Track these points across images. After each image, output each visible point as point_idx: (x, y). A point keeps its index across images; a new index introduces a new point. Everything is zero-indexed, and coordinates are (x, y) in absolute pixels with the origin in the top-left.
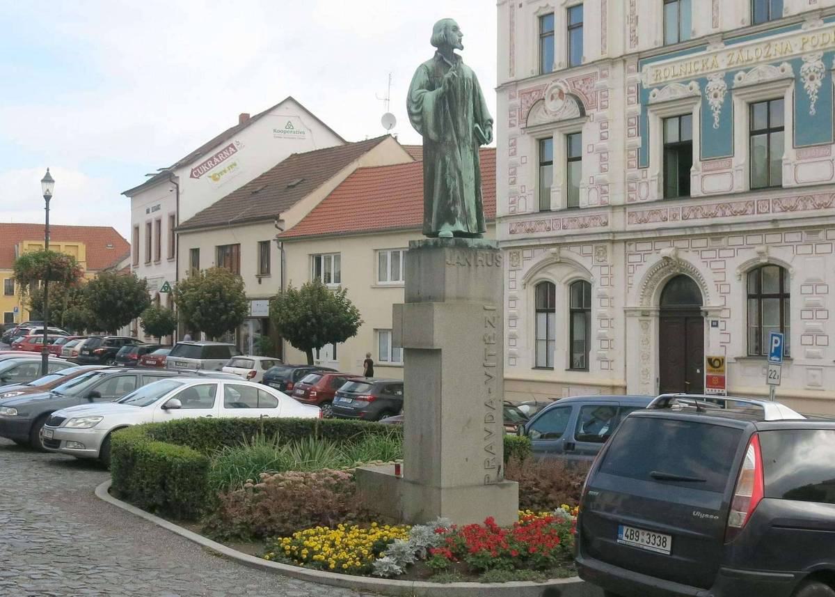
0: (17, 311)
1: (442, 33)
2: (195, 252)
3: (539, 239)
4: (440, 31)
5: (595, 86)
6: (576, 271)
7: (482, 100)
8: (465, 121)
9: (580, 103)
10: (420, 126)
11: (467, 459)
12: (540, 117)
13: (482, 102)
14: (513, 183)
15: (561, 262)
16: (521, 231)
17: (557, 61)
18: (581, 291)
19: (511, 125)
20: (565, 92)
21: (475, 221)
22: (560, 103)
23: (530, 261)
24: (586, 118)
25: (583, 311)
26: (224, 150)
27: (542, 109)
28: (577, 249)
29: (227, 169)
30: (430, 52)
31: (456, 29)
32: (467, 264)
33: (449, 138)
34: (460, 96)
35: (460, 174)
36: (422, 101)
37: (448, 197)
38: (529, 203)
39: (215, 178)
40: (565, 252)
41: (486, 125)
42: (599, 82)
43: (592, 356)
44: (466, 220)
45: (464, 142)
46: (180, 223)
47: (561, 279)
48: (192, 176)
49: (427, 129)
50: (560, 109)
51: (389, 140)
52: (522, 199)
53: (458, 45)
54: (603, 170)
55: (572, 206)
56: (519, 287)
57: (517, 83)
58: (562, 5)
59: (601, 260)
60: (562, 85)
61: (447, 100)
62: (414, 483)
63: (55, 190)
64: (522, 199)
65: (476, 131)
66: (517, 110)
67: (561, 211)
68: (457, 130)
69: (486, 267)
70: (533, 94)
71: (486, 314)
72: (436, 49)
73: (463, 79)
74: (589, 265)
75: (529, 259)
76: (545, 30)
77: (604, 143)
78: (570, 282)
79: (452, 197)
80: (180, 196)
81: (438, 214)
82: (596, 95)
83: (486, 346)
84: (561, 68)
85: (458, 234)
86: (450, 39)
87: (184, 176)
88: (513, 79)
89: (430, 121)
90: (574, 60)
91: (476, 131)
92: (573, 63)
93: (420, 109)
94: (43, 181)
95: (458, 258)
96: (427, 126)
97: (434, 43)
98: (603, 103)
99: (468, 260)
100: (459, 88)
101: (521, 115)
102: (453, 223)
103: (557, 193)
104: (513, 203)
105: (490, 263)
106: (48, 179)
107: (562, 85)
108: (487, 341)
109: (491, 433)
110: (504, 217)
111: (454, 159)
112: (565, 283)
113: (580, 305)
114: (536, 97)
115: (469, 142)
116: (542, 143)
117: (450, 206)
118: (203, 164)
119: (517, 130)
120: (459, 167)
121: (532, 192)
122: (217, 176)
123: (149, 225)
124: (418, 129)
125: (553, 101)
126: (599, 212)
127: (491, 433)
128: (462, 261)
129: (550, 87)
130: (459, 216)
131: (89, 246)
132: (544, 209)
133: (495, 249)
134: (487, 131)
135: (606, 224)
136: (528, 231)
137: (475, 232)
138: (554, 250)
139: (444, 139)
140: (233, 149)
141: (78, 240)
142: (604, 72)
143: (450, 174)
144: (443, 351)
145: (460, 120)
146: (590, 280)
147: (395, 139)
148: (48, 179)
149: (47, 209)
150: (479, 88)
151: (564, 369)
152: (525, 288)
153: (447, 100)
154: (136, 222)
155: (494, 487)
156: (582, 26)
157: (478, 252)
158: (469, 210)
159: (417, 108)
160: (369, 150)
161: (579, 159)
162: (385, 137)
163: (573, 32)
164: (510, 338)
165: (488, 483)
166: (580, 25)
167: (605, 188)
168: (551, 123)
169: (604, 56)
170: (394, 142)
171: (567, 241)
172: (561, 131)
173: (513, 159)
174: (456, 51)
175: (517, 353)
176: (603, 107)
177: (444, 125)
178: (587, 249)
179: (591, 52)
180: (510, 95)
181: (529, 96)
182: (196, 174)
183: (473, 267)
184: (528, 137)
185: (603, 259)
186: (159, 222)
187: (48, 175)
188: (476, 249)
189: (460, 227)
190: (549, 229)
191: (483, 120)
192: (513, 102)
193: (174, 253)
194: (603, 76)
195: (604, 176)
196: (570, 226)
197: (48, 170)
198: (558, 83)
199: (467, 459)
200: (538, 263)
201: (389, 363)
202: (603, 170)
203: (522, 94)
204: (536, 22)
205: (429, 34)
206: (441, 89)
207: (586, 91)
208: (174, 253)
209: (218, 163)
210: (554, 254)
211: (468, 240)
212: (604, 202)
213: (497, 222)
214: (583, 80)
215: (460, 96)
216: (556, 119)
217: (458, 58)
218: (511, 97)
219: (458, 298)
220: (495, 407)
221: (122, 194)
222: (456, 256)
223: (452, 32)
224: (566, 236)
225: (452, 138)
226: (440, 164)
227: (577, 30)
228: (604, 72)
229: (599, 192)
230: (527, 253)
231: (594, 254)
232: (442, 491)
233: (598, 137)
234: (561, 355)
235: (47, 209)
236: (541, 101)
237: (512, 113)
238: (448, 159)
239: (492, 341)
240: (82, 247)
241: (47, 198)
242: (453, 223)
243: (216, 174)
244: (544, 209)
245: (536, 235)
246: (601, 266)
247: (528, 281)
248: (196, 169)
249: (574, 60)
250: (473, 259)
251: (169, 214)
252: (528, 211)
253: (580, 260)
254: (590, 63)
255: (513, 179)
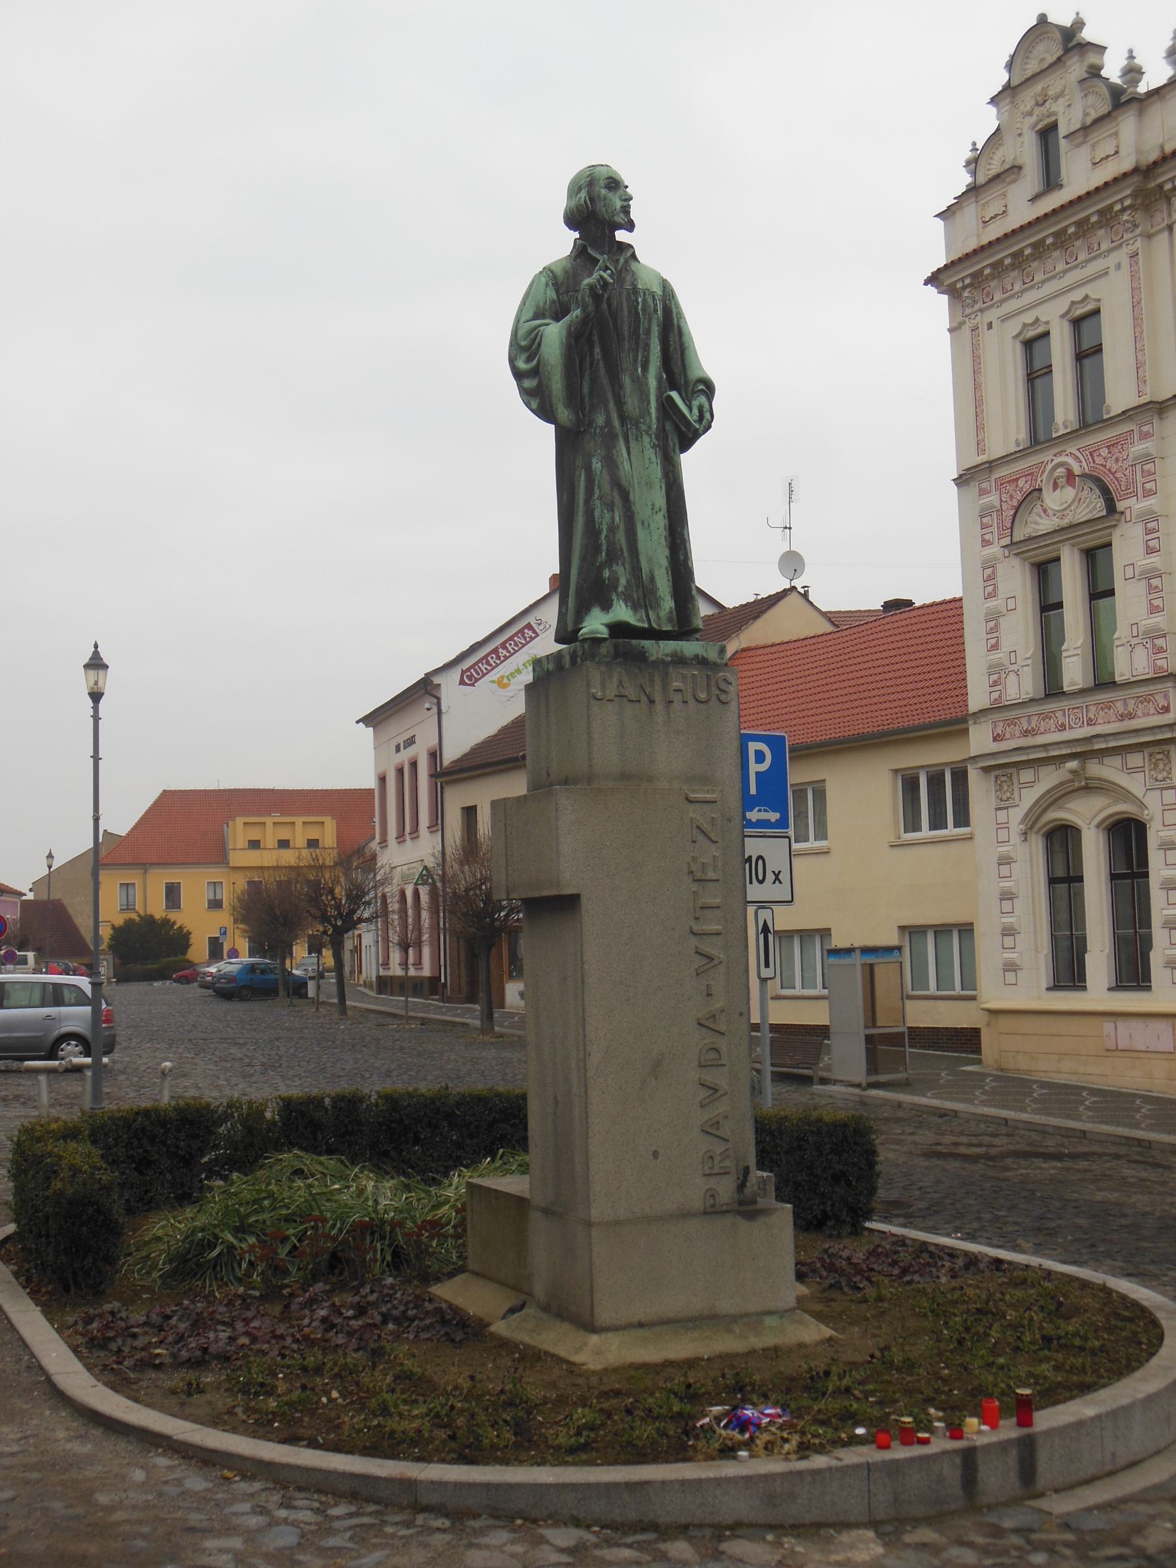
0: (225, 933)
1: (583, 194)
2: (470, 813)
3: (1045, 746)
4: (580, 189)
5: (1131, 456)
6: (1116, 801)
7: (685, 339)
8: (640, 385)
9: (1106, 492)
10: (538, 401)
11: (656, 1154)
12: (1040, 523)
13: (684, 330)
14: (995, 647)
15: (1091, 787)
16: (1013, 736)
17: (1059, 418)
18: (1128, 837)
19: (986, 543)
20: (1077, 470)
21: (668, 604)
22: (1069, 493)
23: (1032, 790)
24: (1117, 516)
25: (1132, 876)
26: (516, 635)
27: (1038, 509)
28: (1116, 761)
29: (521, 667)
30: (564, 242)
31: (614, 184)
32: (644, 699)
33: (600, 420)
34: (626, 327)
35: (625, 496)
36: (539, 345)
37: (597, 549)
38: (1024, 683)
39: (501, 683)
40: (1095, 769)
41: (694, 392)
42: (1138, 448)
43: (1156, 959)
44: (643, 597)
45: (637, 428)
46: (446, 763)
47: (1088, 816)
48: (462, 682)
49: (551, 403)
50: (1069, 506)
51: (793, 598)
52: (1012, 676)
53: (621, 218)
54: (1154, 610)
55: (1103, 682)
56: (1016, 839)
57: (991, 465)
58: (1062, 316)
59: (1160, 777)
60: (1070, 460)
61: (596, 338)
62: (547, 1212)
63: (111, 683)
64: (1012, 676)
65: (667, 407)
66: (995, 515)
67: (1083, 692)
68: (620, 403)
69: (692, 702)
70: (1021, 483)
71: (693, 812)
72: (577, 235)
73: (635, 290)
74: (1136, 785)
75: (1030, 784)
76: (1038, 365)
77: (1154, 559)
78: (1108, 822)
79: (604, 548)
80: (444, 717)
81: (579, 590)
82: (1134, 473)
83: (695, 887)
84: (1069, 430)
85: (619, 630)
86: (600, 206)
87: (449, 685)
88: (983, 458)
89: (557, 384)
90: (1091, 416)
91: (667, 407)
92: (1090, 420)
93: (535, 362)
94: (86, 666)
95: (621, 684)
96: (550, 397)
97: (573, 220)
98: (1148, 486)
99: (648, 690)
100: (626, 312)
101: (1002, 527)
102: (606, 607)
103: (1075, 658)
104: (995, 683)
105: (703, 696)
106: (96, 663)
107: (1070, 460)
108: (699, 875)
109: (716, 1090)
110: (980, 711)
111: (611, 464)
112: (1098, 826)
113: (1129, 865)
114: (1027, 488)
115: (650, 427)
116: (1044, 572)
117: (600, 569)
118: (480, 661)
119: (995, 550)
120: (624, 483)
121: (1029, 662)
122: (505, 681)
123: (400, 771)
124: (534, 406)
125: (1058, 490)
126: (1152, 688)
127: (716, 1090)
128: (631, 692)
129: (1050, 466)
130: (620, 589)
131: (342, 819)
132: (1053, 689)
133: (715, 664)
134: (695, 403)
135: (1166, 709)
136: (1026, 733)
137: (667, 627)
138: (1073, 764)
139: (591, 422)
140: (530, 633)
141: (321, 812)
142: (1145, 429)
143: (600, 498)
144: (583, 900)
145: (626, 381)
146: (1144, 816)
147: (805, 596)
148: (96, 663)
149: (96, 718)
150: (680, 315)
151: (1107, 986)
152: (1026, 840)
153: (596, 338)
154: (381, 770)
155: (728, 1220)
156: (1101, 350)
157: (671, 670)
158: (652, 579)
159: (529, 360)
160: (758, 617)
161: (1111, 593)
162: (784, 594)
163: (1086, 362)
164: (1003, 935)
165: (712, 1212)
166: (1098, 349)
167: (1160, 642)
168: (1055, 531)
169: (1145, 399)
170: (802, 600)
171: (1097, 747)
172: (1073, 545)
173: (992, 603)
174: (621, 236)
175: (1018, 962)
176: (1148, 494)
177: (591, 392)
178: (1135, 759)
179: (1120, 393)
180: (980, 490)
181: (1013, 486)
182: (470, 678)
183: (659, 706)
184: (1016, 562)
185: (1165, 774)
186: (414, 765)
187: (96, 655)
188: (665, 664)
189: (622, 612)
190: (1062, 728)
191: (687, 382)
192: (986, 500)
193: (438, 821)
194: (1145, 436)
195: (1157, 620)
196: (1103, 722)
197: (96, 646)
198: (1063, 459)
199: (656, 1154)
200: (1048, 791)
201: (798, 991)
202: (1154, 610)
203: (1001, 484)
204: (1019, 348)
205: (560, 203)
206: (576, 313)
207: (1114, 468)
208: (438, 821)
209: (506, 658)
210: (1073, 772)
211: (647, 643)
212: (1161, 668)
213: (970, 722)
214: (1108, 447)
215: (626, 327)
216: (1065, 522)
217: (624, 248)
218: (983, 492)
219: (625, 776)
220: (723, 1028)
221: (358, 722)
222: (615, 680)
223: (603, 191)
224: (1093, 737)
225: (608, 421)
226: (583, 478)
227: (1094, 359)
228: (1145, 429)
229: (1150, 651)
230: (1026, 775)
231: (1147, 769)
232: (595, 1232)
233: (1141, 549)
234: (1099, 961)
235: (96, 718)
236: (1036, 494)
237: (985, 520)
238: (597, 465)
239: (711, 875)
240: (330, 824)
241: (96, 696)
242: (606, 607)
243: (502, 677)
244: (1053, 689)
245: (1041, 740)
246: (1162, 789)
247: (1031, 828)
248: (468, 670)
249: (1091, 416)
250: (658, 687)
251: (428, 751)
252: (1025, 697)
253: (1122, 780)
254: (1119, 415)
255: (993, 641)
